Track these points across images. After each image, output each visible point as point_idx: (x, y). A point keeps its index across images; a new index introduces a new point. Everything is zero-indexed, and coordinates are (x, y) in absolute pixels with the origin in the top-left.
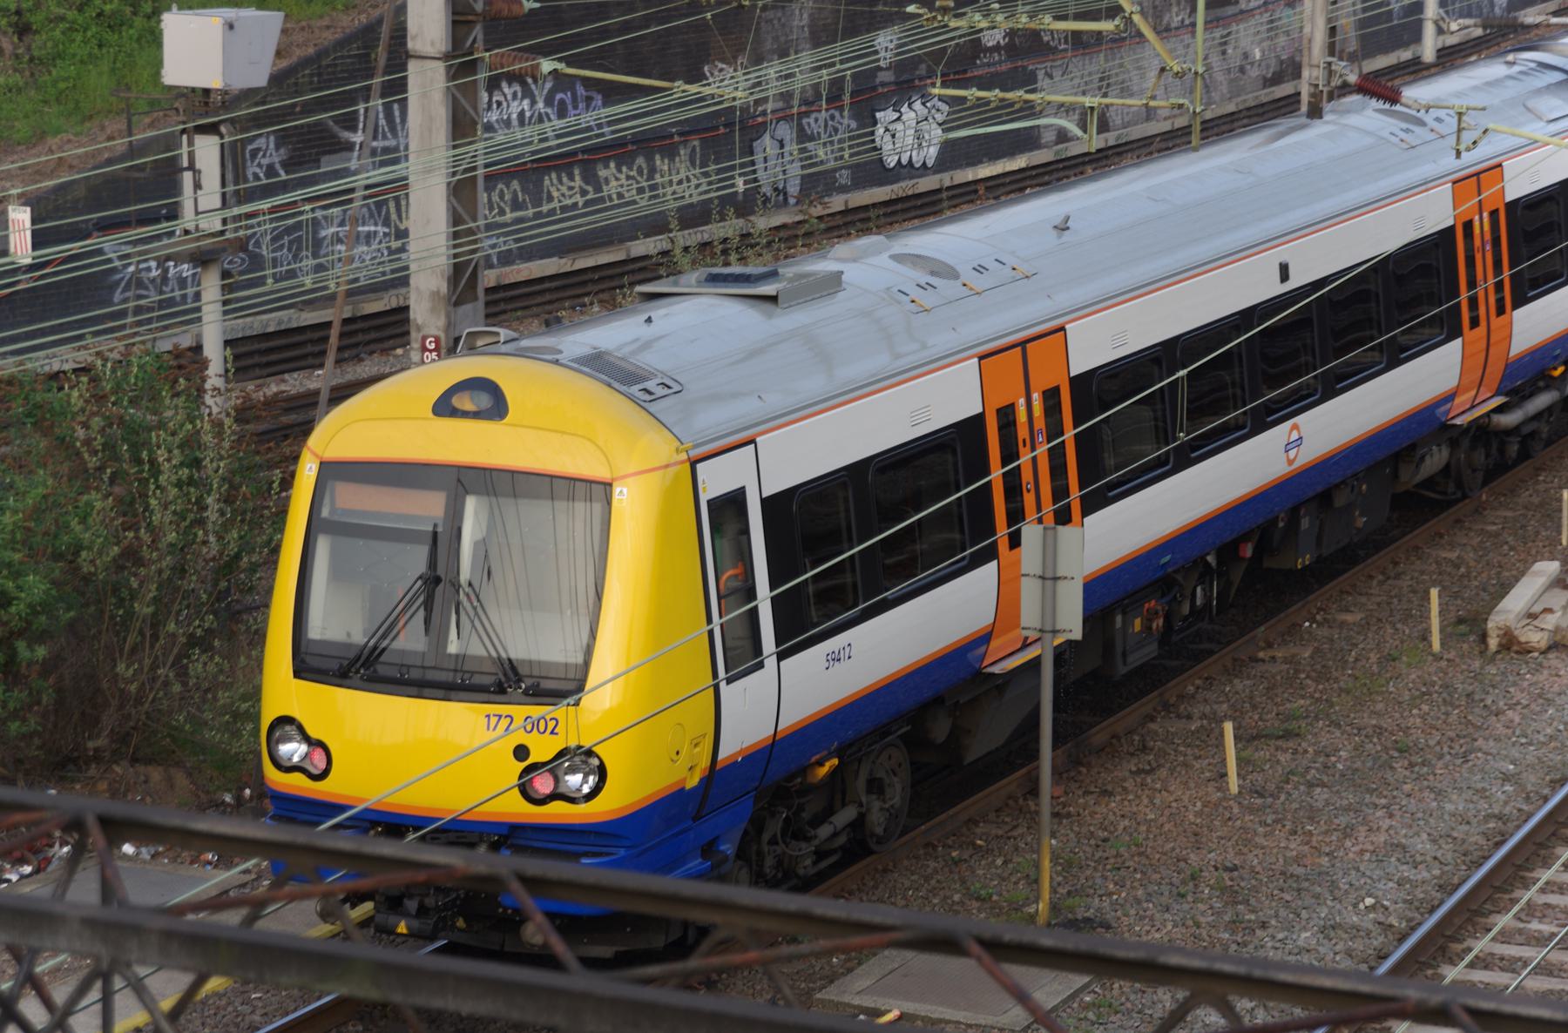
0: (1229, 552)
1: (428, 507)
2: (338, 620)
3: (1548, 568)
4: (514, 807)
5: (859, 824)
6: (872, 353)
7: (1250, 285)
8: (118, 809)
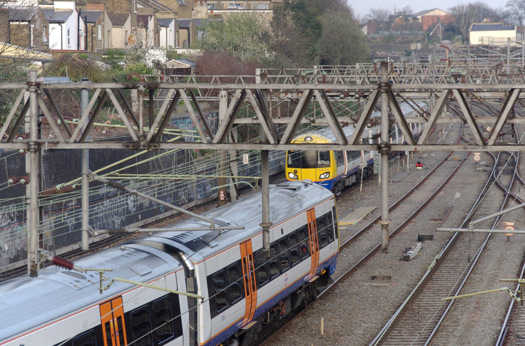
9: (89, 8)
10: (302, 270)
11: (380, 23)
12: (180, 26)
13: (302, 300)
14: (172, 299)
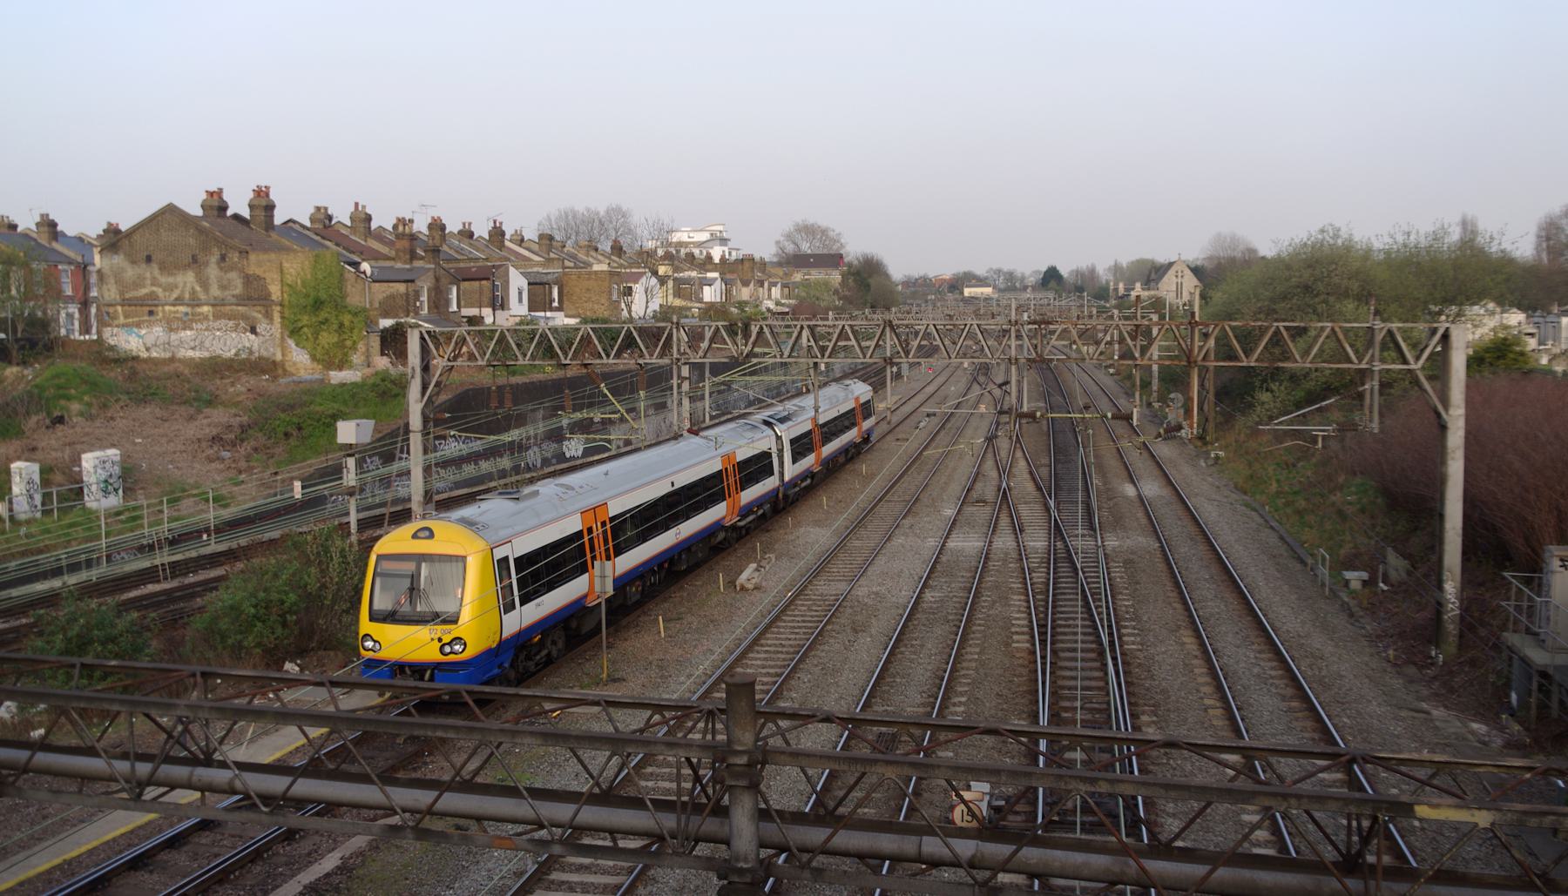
0: (661, 566)
1: (410, 567)
2: (383, 603)
3: (754, 566)
4: (439, 658)
5: (549, 655)
6: (547, 514)
7: (667, 489)
8: (208, 669)
9: (728, 276)
10: (213, 573)
11: (907, 283)
12: (784, 286)
13: (852, 454)
14: (766, 455)
